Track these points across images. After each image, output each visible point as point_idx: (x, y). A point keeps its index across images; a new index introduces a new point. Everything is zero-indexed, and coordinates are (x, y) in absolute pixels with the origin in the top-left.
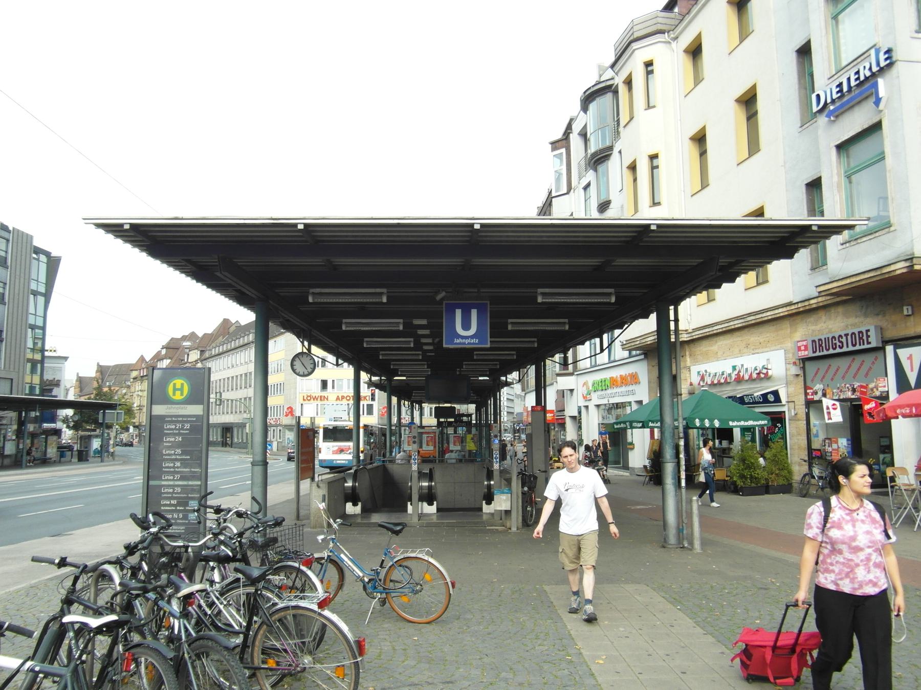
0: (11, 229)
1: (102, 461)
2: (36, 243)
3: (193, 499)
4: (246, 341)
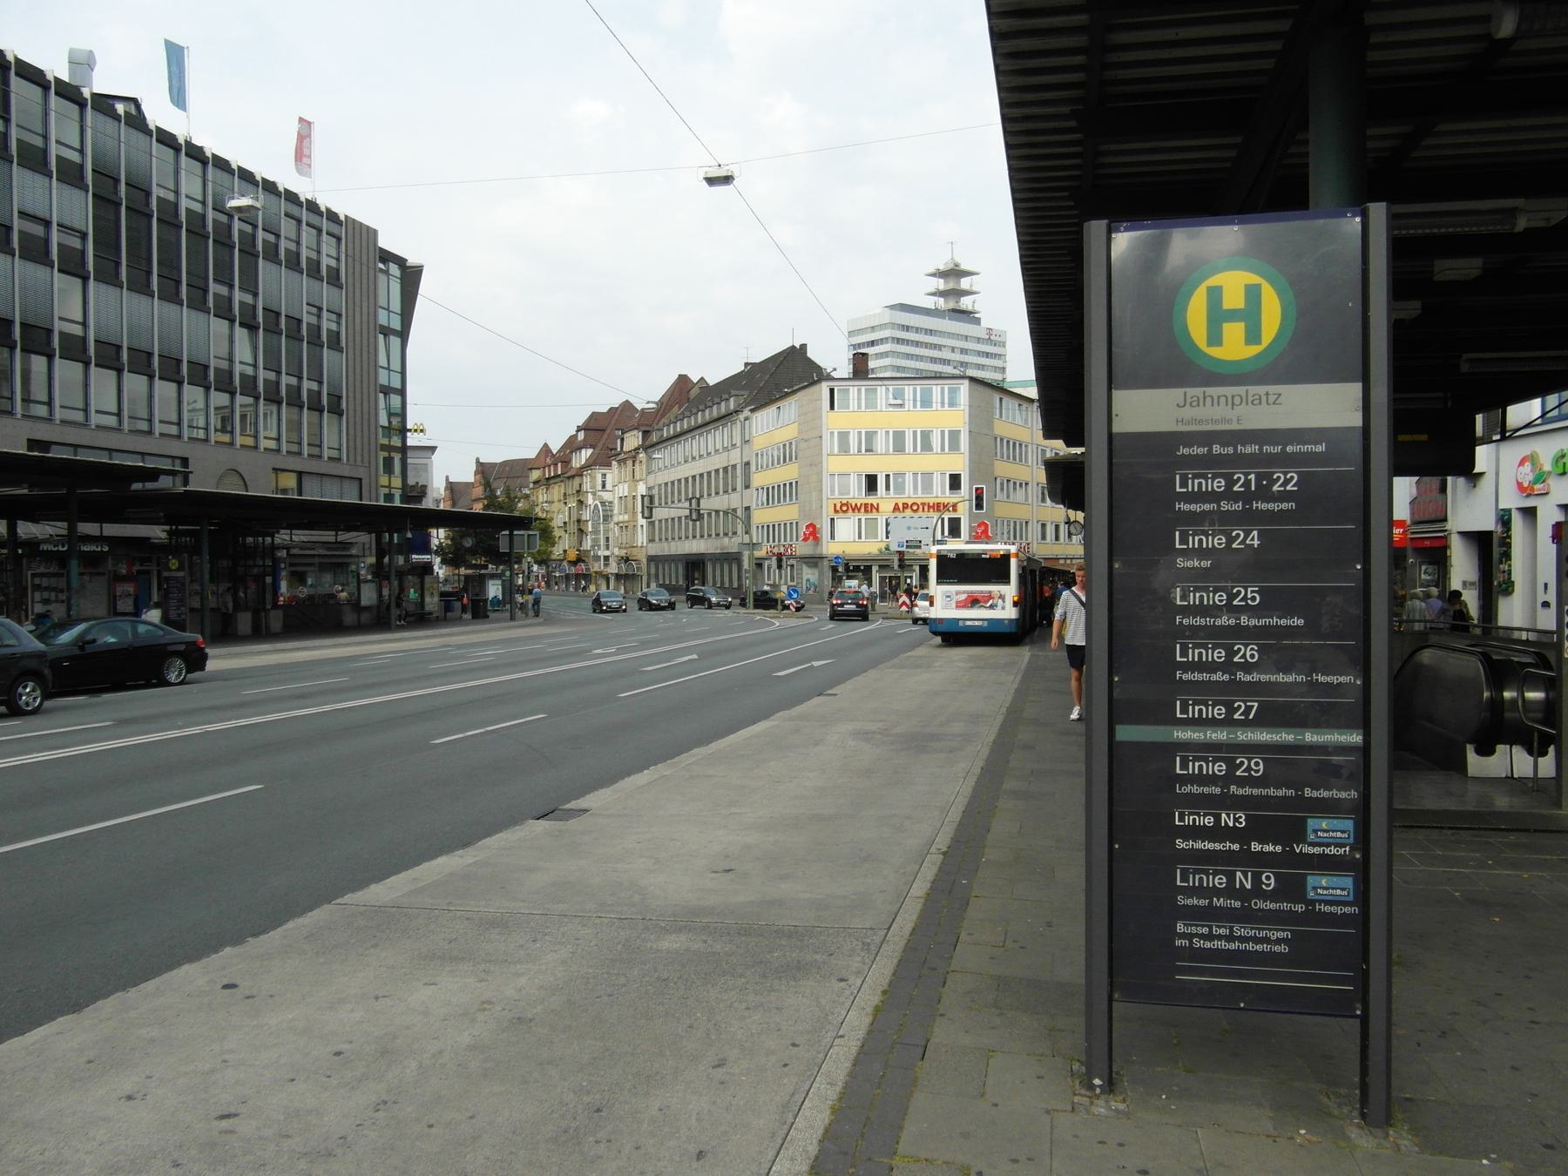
0: (342, 218)
1: (512, 618)
2: (384, 242)
3: (1328, 808)
4: (723, 410)
